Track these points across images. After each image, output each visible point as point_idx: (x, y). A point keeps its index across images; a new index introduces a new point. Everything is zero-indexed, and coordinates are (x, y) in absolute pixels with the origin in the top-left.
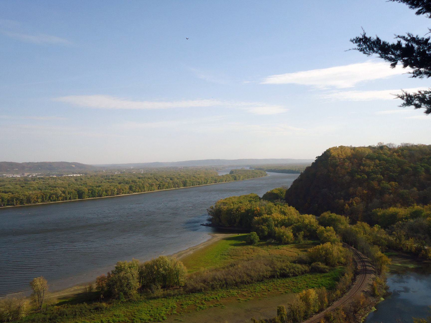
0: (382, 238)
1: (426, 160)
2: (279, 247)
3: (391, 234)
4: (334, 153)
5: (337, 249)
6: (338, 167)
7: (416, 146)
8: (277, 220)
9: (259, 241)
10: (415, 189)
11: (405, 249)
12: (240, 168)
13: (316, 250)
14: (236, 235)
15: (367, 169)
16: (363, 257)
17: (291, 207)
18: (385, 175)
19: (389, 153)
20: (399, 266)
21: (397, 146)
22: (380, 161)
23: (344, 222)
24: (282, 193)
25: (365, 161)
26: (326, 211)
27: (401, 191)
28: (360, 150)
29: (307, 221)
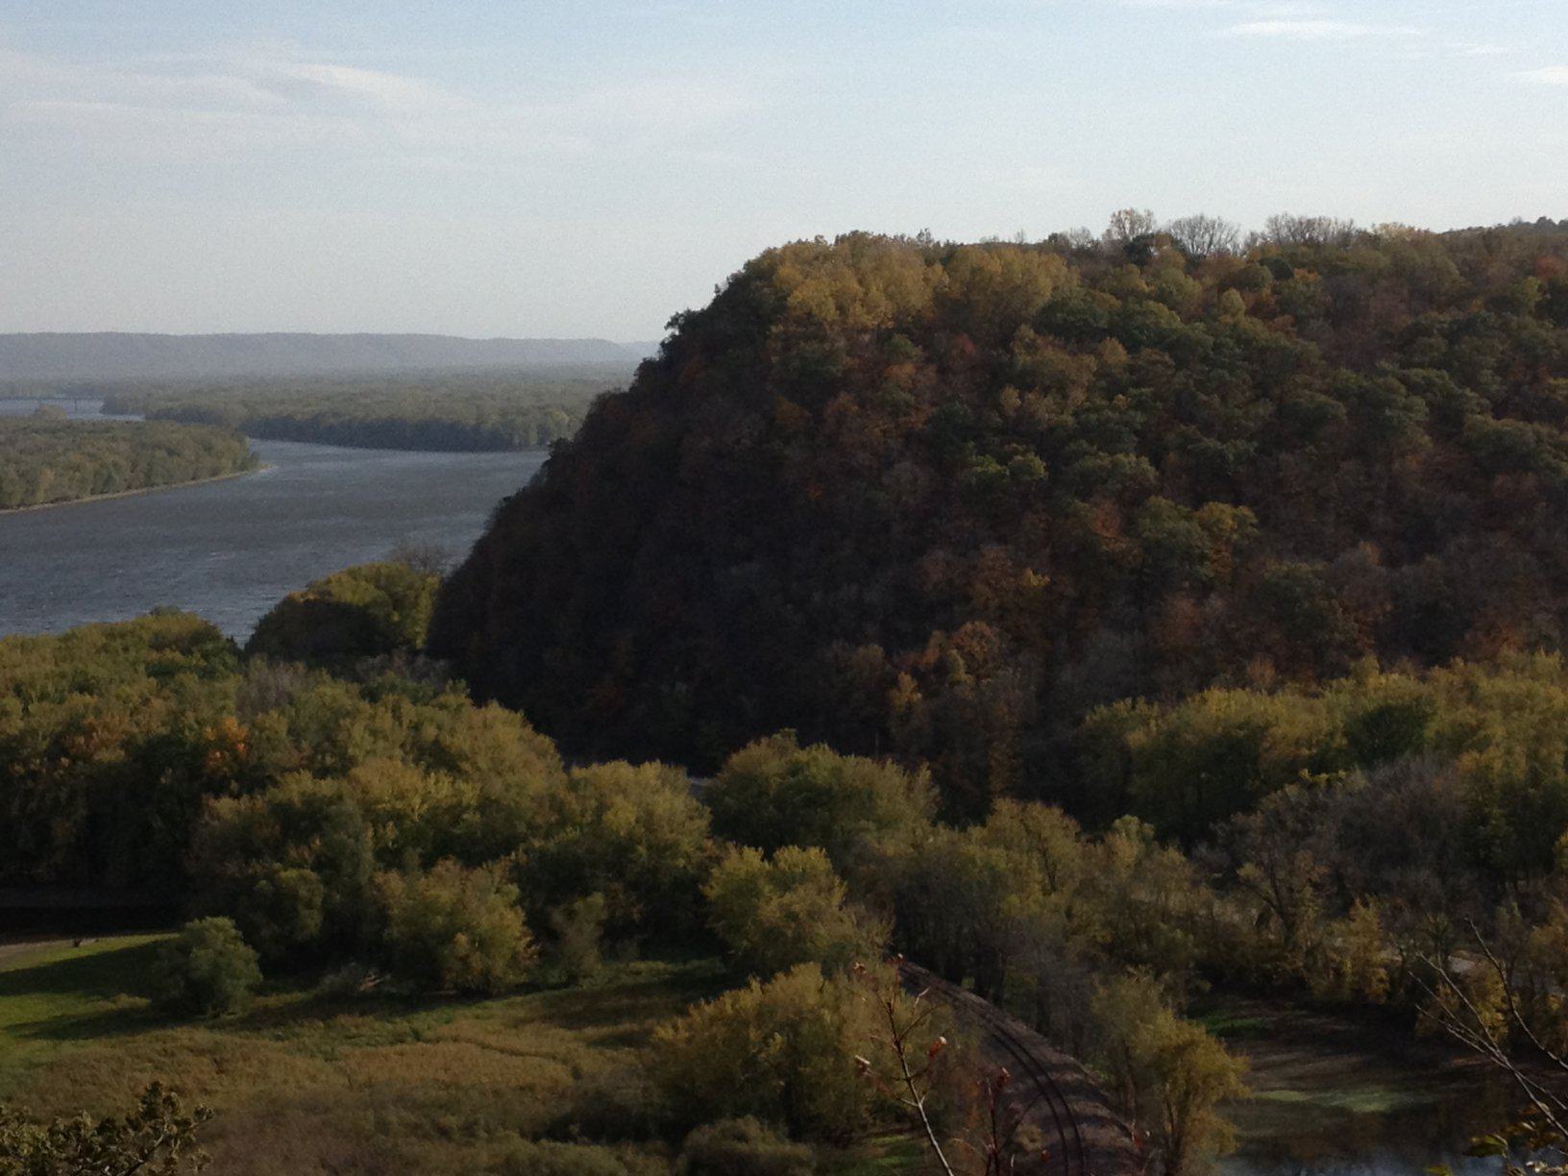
0: (1165, 915)
1: (1440, 343)
2: (422, 1020)
3: (1226, 882)
4: (810, 293)
5: (862, 1012)
6: (844, 398)
7: (1370, 240)
8: (398, 817)
9: (258, 990)
10: (1368, 552)
11: (1320, 984)
12: (24, 407)
13: (720, 1031)
14: (58, 951)
15: (1044, 408)
16: (1051, 1055)
17: (495, 711)
18: (1173, 457)
19: (1193, 287)
20: (1294, 1106)
21: (1241, 241)
22: (1132, 347)
23: (897, 806)
24: (398, 603)
25: (1031, 347)
26: (764, 727)
27: (1274, 568)
28: (995, 266)
29: (623, 816)
